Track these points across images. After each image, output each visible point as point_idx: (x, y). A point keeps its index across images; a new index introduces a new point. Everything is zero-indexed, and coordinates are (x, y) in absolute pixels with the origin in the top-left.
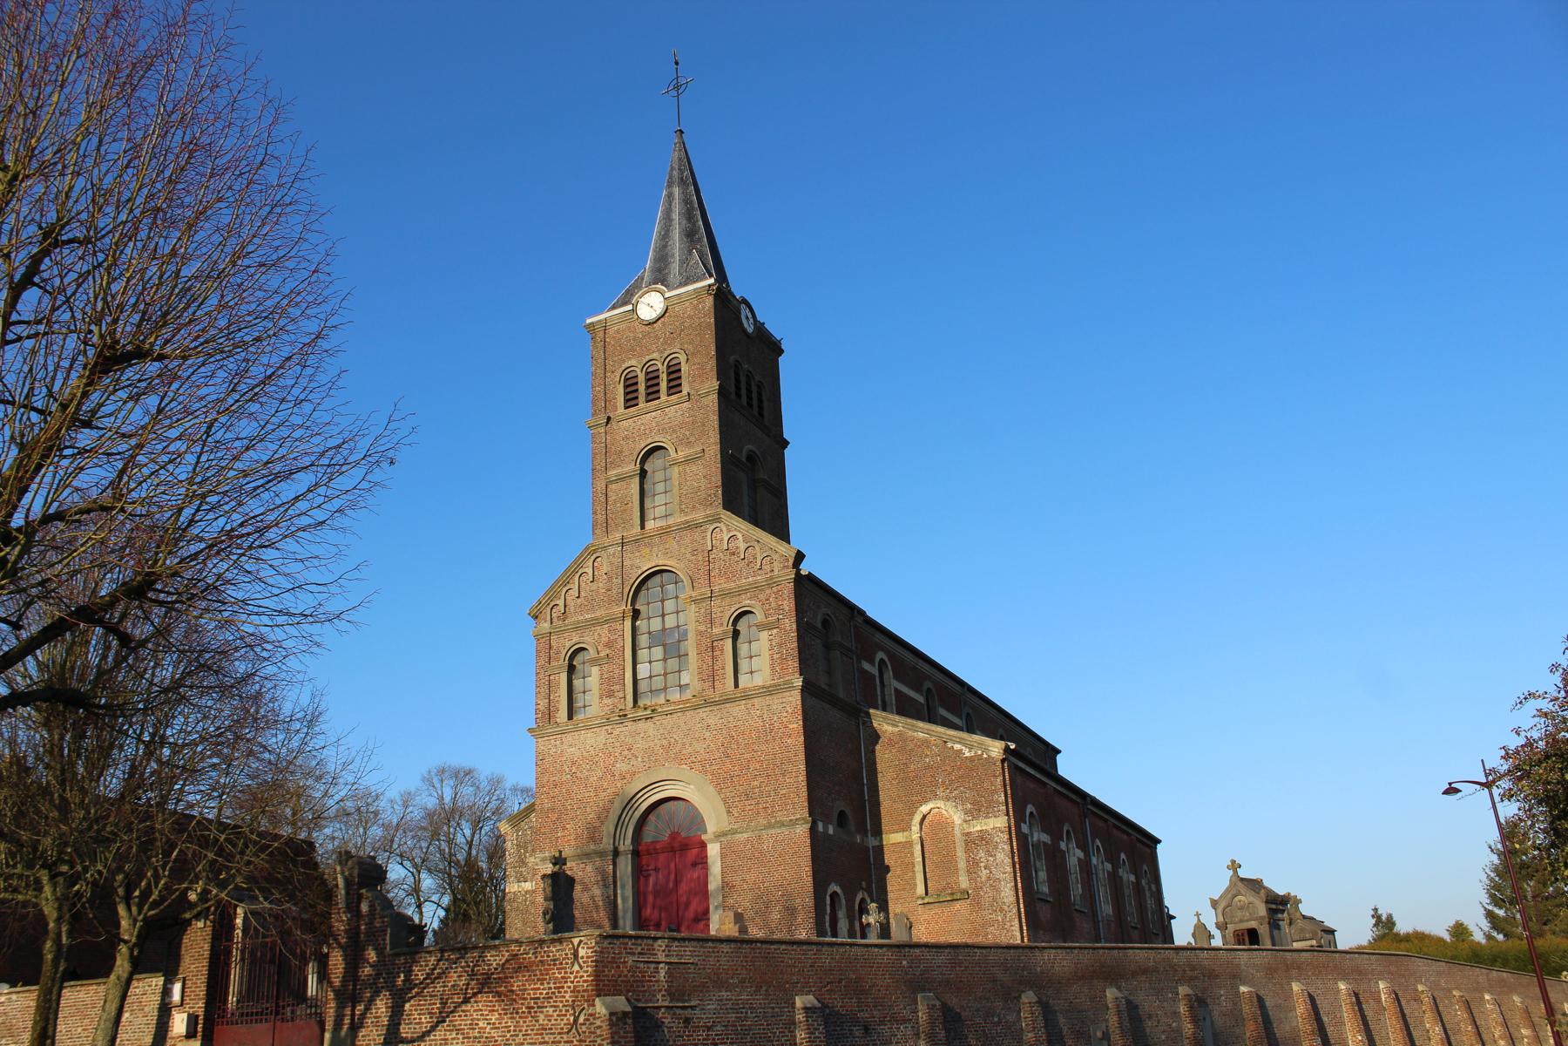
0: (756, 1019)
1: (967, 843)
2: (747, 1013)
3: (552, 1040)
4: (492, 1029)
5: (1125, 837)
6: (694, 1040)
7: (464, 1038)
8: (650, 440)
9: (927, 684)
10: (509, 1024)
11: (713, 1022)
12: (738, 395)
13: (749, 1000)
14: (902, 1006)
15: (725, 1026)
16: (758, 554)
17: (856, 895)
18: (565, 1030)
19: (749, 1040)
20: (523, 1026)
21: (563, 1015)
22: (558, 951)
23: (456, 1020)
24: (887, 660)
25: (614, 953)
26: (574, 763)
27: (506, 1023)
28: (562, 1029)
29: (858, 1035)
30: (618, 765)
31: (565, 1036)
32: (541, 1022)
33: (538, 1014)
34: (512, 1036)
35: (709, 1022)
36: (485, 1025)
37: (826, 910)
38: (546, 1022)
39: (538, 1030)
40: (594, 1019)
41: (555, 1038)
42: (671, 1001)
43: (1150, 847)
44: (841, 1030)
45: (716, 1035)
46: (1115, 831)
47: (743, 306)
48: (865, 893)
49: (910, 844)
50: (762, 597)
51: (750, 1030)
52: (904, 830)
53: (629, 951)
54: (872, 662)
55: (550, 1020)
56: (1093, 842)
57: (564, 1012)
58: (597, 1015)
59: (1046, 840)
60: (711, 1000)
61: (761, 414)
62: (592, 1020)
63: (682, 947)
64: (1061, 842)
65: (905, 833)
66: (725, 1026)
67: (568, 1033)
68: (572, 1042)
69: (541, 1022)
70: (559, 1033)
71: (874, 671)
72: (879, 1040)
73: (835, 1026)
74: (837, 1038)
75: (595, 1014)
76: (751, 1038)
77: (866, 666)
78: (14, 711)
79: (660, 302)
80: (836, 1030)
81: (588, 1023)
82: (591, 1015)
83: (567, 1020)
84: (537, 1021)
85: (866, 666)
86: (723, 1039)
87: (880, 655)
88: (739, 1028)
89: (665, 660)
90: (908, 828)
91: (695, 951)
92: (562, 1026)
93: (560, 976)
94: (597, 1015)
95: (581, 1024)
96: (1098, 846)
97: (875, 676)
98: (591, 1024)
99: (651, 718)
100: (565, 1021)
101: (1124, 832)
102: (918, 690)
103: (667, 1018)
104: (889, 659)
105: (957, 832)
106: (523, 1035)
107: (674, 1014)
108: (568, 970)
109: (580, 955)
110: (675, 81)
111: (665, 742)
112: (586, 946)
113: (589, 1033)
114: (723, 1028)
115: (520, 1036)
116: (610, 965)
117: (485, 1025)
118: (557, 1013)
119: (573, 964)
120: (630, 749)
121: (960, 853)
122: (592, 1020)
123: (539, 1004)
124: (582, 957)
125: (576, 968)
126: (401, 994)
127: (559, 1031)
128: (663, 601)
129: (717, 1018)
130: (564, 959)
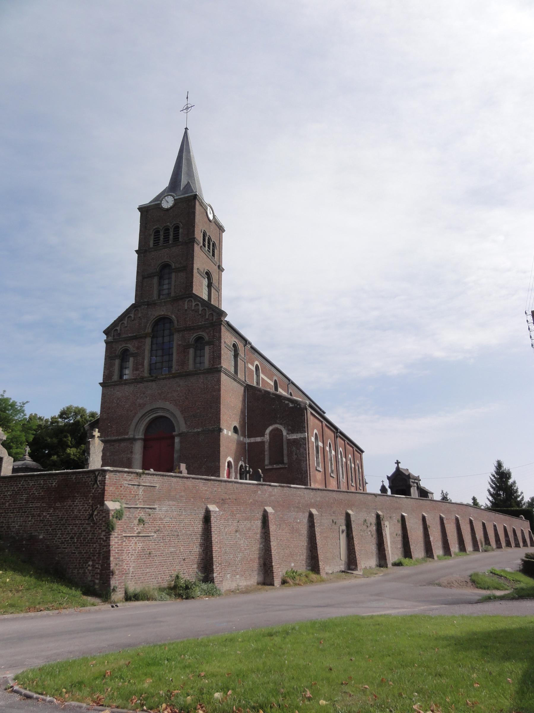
0: (187, 515)
1: (288, 443)
2: (182, 512)
3: (80, 523)
4: (50, 516)
5: (351, 448)
6: (155, 525)
7: (35, 521)
8: (163, 261)
9: (275, 378)
10: (59, 514)
11: (165, 516)
12: (204, 245)
13: (184, 506)
14: (256, 512)
15: (171, 518)
16: (207, 313)
17: (239, 463)
18: (87, 518)
19: (182, 525)
20: (66, 515)
21: (86, 510)
22: (87, 477)
23: (32, 512)
24: (259, 365)
25: (116, 479)
26: (118, 399)
27: (57, 513)
28: (86, 517)
29: (235, 525)
30: (138, 400)
31: (87, 521)
32: (75, 513)
33: (74, 509)
34: (59, 520)
35: (163, 516)
36: (47, 514)
37: (225, 469)
38: (78, 514)
39: (73, 517)
40: (102, 512)
41: (81, 522)
42: (144, 505)
43: (360, 454)
44: (227, 522)
45: (166, 523)
46: (347, 445)
47: (209, 208)
48: (243, 462)
49: (263, 443)
50: (207, 331)
51: (183, 521)
52: (261, 436)
53: (124, 478)
54: (253, 365)
55: (80, 513)
56: (339, 448)
57: (87, 509)
58: (104, 511)
59: (321, 445)
60: (165, 505)
61: (213, 255)
62: (101, 513)
63: (152, 478)
64: (327, 447)
65: (262, 438)
66: (171, 518)
67: (88, 519)
68: (90, 524)
69: (75, 513)
70: (84, 520)
71: (254, 369)
72: (245, 528)
73: (225, 520)
74: (225, 526)
75: (103, 510)
76: (183, 524)
77: (250, 366)
78: (21, 446)
79: (172, 201)
80: (225, 522)
81: (99, 514)
82: (101, 510)
83: (89, 512)
84: (73, 513)
85: (250, 366)
86: (169, 525)
87: (256, 363)
88: (178, 520)
89: (162, 356)
90: (263, 435)
91: (158, 480)
92: (86, 516)
93: (87, 490)
94: (104, 511)
95: (95, 515)
96: (341, 451)
97: (253, 371)
98: (101, 515)
99: (155, 380)
100: (88, 513)
101: (351, 446)
102: (271, 380)
103: (141, 513)
104: (260, 365)
105: (284, 437)
106: (65, 520)
107: (145, 511)
108: (91, 487)
109: (98, 480)
110: (188, 111)
111: (160, 391)
112: (102, 475)
113: (99, 519)
114: (170, 519)
115: (64, 521)
116: (113, 486)
117: (47, 514)
118: (84, 509)
119: (94, 484)
120: (144, 394)
121: (285, 447)
122: (101, 513)
123: (75, 504)
124: (99, 481)
125: (95, 486)
126: (5, 498)
127: (84, 518)
128: (164, 330)
129: (167, 514)
130: (90, 482)
